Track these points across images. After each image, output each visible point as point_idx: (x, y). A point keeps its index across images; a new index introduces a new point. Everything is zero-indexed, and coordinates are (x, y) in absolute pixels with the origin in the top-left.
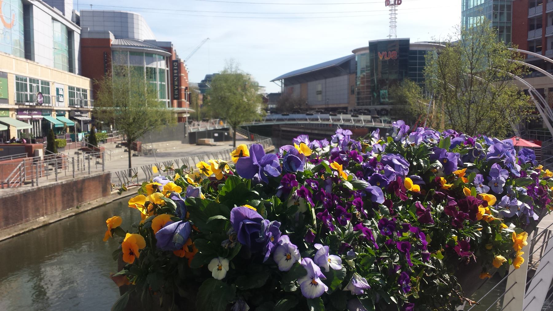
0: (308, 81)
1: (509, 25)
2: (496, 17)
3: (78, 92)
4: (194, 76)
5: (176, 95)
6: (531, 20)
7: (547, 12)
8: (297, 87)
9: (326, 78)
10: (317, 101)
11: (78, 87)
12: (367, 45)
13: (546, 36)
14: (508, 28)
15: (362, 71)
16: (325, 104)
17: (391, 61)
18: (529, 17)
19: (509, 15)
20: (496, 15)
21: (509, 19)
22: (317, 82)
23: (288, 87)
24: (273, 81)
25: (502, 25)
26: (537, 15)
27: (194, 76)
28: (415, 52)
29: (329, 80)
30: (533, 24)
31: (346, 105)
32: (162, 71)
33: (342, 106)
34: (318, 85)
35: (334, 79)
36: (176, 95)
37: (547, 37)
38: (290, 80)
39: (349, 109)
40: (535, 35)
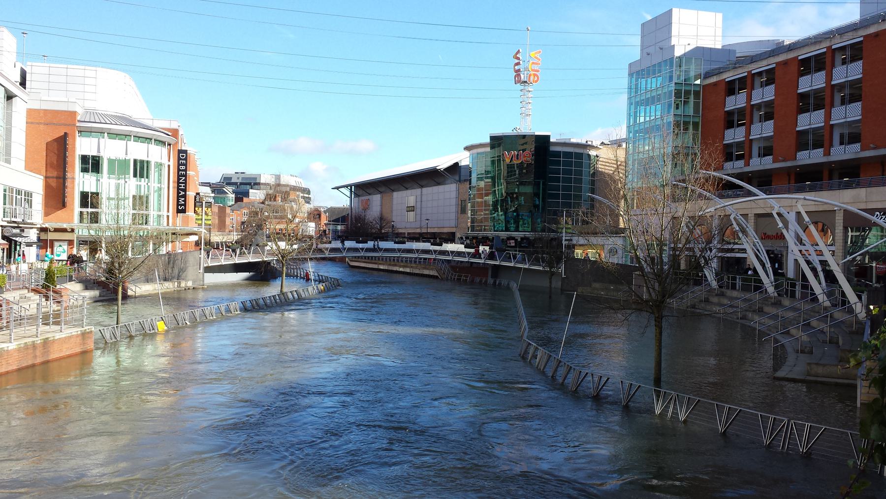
0: (393, 191)
1: (697, 120)
2: (677, 108)
3: (19, 197)
4: (207, 169)
5: (181, 205)
6: (730, 113)
7: (833, 83)
8: (376, 199)
9: (422, 187)
10: (405, 221)
11: (20, 187)
12: (488, 140)
13: (832, 123)
14: (696, 125)
15: (479, 179)
16: (421, 228)
17: (520, 166)
18: (799, 91)
19: (696, 105)
20: (677, 105)
21: (696, 110)
22: (409, 192)
23: (361, 198)
24: (337, 188)
25: (687, 119)
26: (850, 79)
27: (207, 169)
28: (557, 154)
29: (426, 190)
30: (731, 120)
31: (453, 230)
32: (159, 165)
33: (445, 230)
34: (409, 197)
35: (436, 189)
36: (181, 205)
37: (832, 125)
38: (362, 189)
39: (458, 235)
40: (735, 135)
